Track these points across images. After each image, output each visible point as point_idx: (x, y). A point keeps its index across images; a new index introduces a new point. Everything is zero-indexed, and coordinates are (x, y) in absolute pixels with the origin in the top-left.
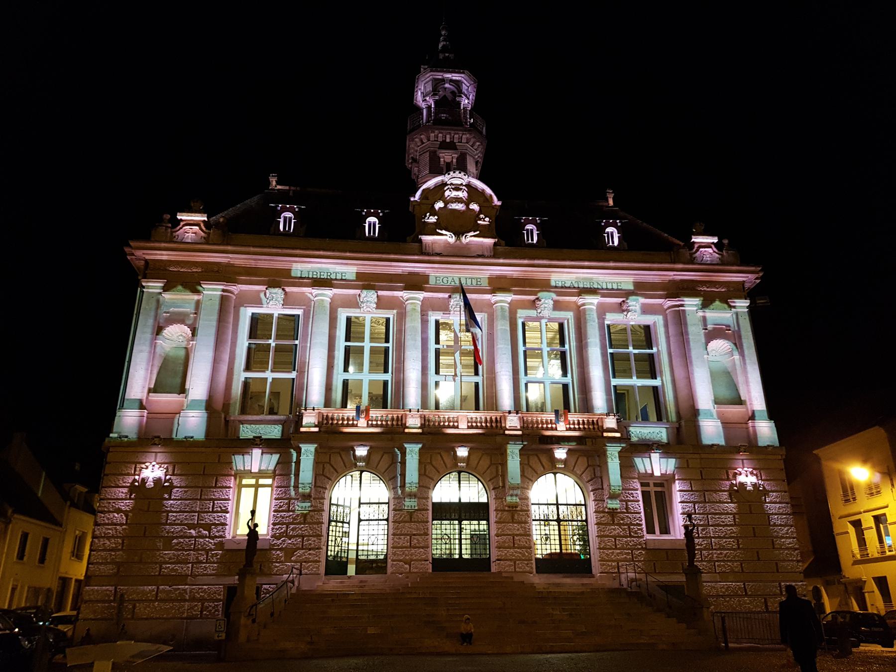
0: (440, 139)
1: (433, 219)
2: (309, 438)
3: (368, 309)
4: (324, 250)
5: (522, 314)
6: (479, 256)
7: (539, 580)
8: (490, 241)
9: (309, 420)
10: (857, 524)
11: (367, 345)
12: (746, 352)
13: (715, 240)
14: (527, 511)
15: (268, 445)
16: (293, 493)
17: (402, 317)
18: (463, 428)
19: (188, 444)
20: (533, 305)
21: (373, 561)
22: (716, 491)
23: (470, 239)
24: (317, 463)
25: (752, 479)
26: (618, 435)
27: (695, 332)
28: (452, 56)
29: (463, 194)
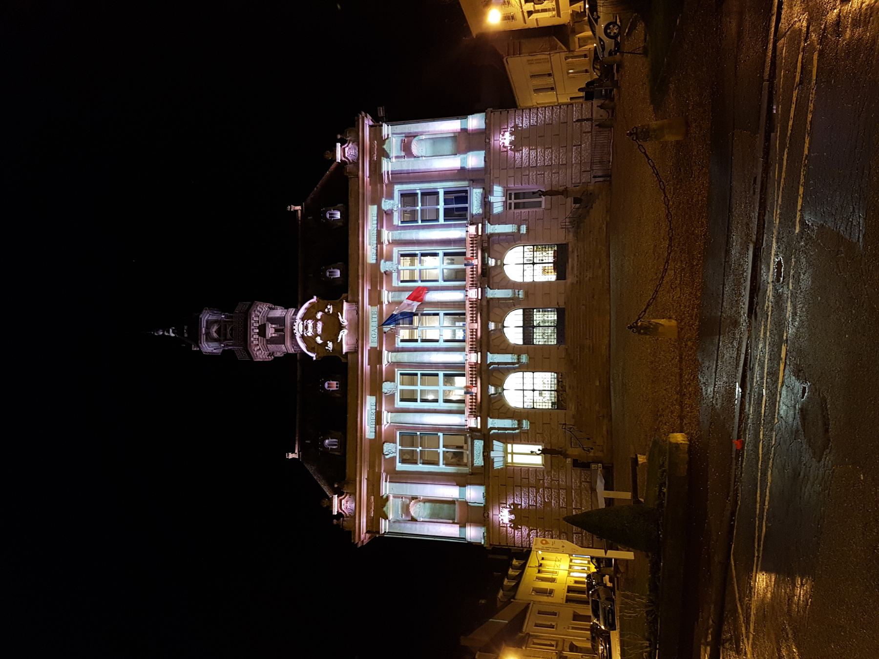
0: (257, 336)
1: (330, 344)
2: (484, 423)
3: (394, 387)
4: (357, 418)
5: (396, 283)
6: (358, 313)
7: (570, 279)
8: (345, 305)
9: (473, 423)
10: (530, 13)
11: (419, 388)
12: (420, 130)
13: (339, 145)
14: (529, 284)
15: (488, 448)
16: (517, 431)
17: (399, 364)
18: (477, 326)
19: (487, 496)
20: (388, 274)
21: (558, 381)
22: (515, 161)
23: (344, 319)
24: (499, 417)
25: (507, 134)
26: (480, 225)
27: (407, 165)
28: (186, 327)
29: (310, 323)
